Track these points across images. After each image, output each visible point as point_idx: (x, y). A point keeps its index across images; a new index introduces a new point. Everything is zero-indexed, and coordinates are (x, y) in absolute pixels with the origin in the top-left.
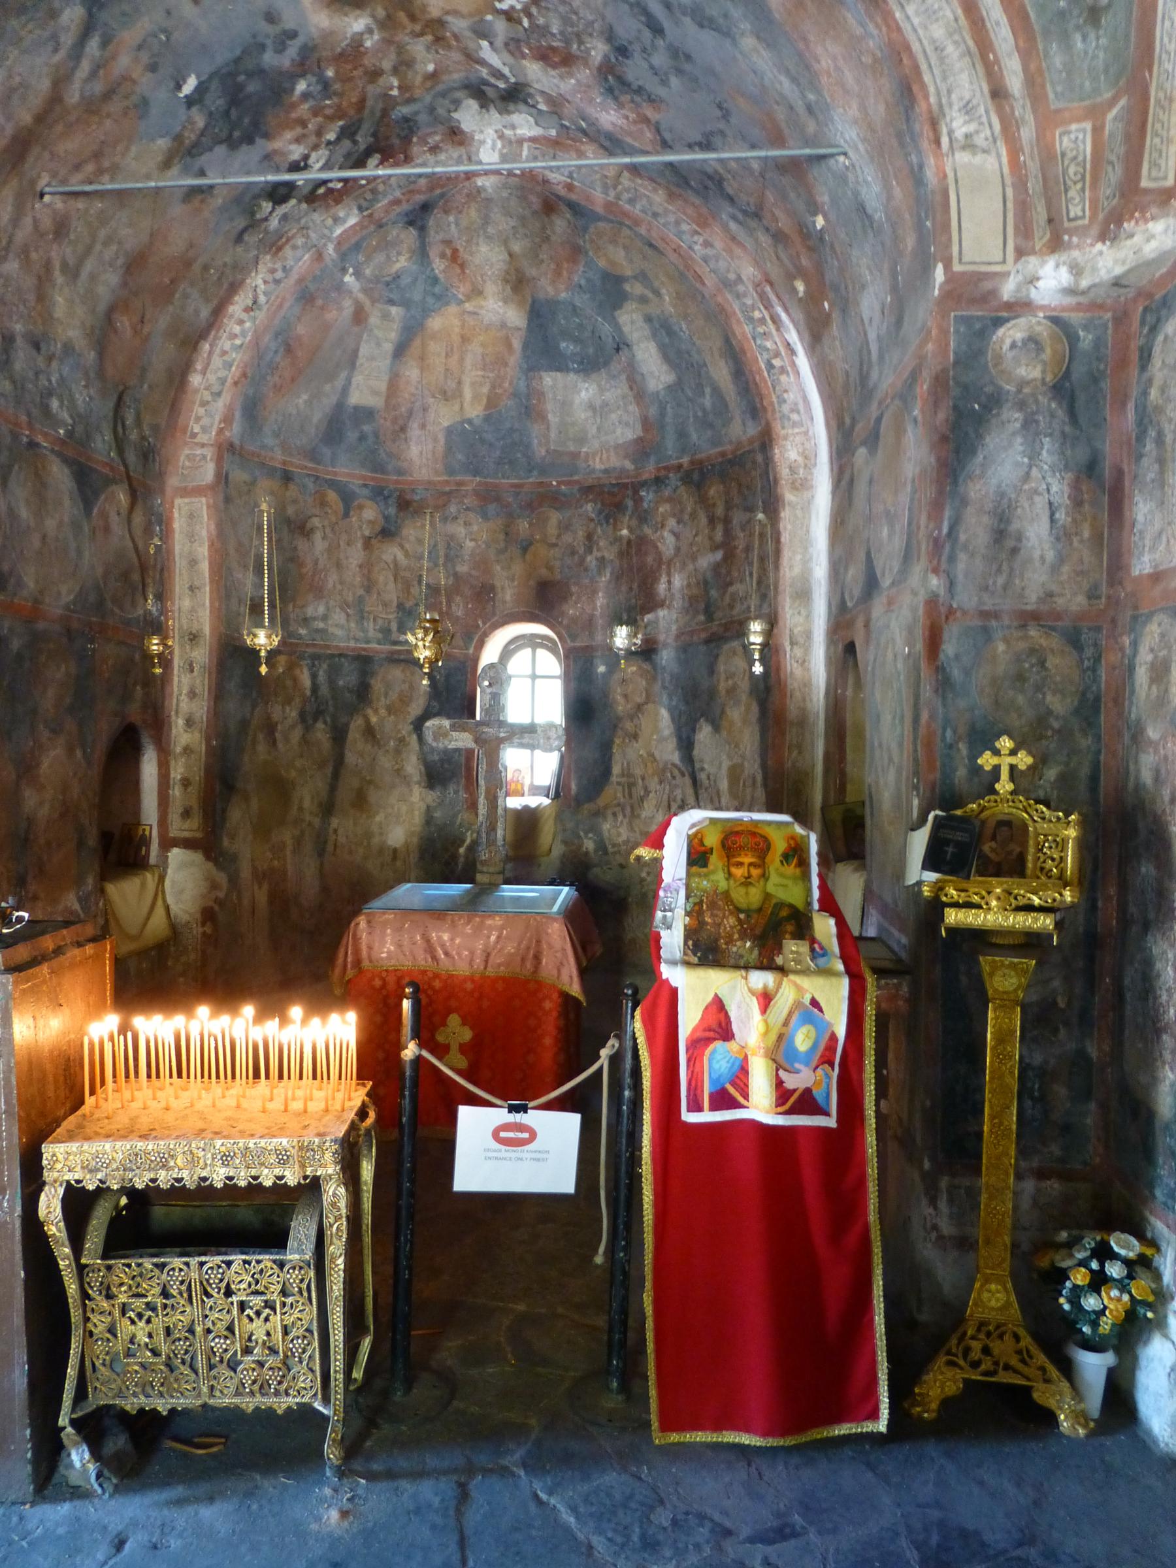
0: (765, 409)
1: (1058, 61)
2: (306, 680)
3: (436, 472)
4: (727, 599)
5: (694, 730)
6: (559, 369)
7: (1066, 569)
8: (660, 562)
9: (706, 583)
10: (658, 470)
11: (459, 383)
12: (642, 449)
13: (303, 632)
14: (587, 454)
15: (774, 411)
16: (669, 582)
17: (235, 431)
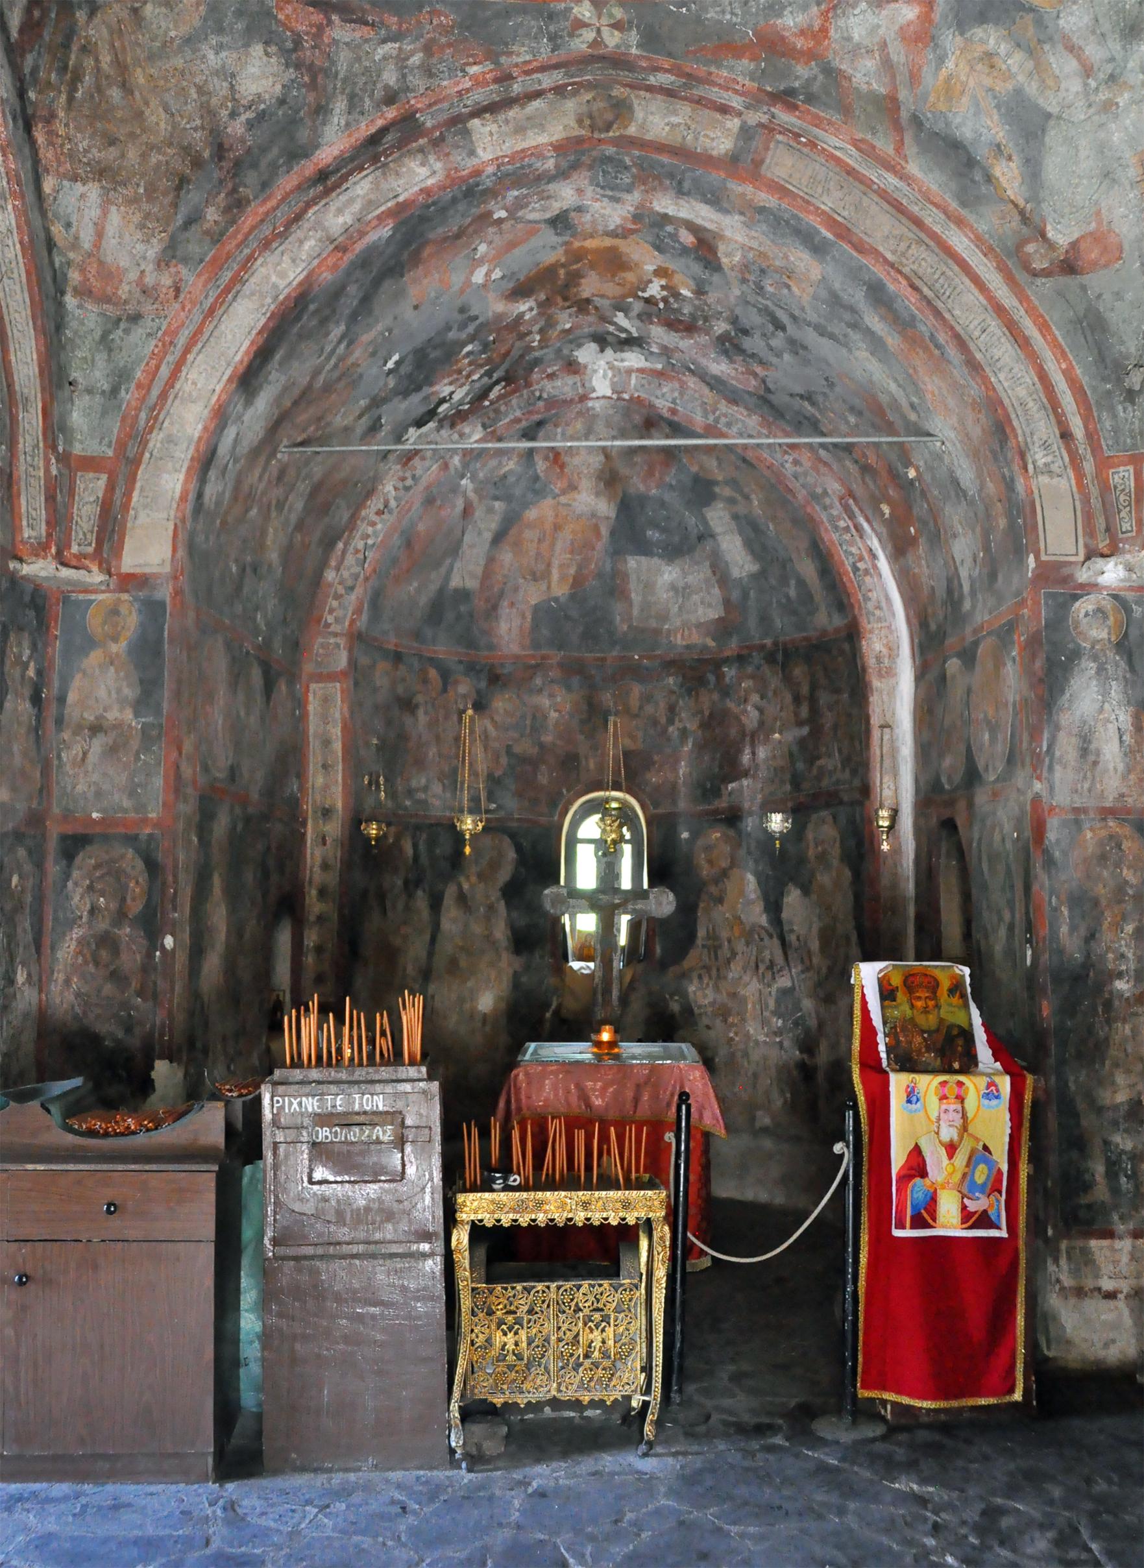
0: (852, 606)
1: (1108, 424)
2: (409, 850)
3: (523, 647)
4: (815, 771)
5: (782, 894)
6: (646, 554)
7: (1132, 777)
8: (744, 735)
9: (791, 755)
10: (741, 648)
11: (549, 565)
12: (723, 628)
13: (408, 803)
14: (669, 631)
15: (860, 608)
16: (754, 753)
17: (363, 622)
